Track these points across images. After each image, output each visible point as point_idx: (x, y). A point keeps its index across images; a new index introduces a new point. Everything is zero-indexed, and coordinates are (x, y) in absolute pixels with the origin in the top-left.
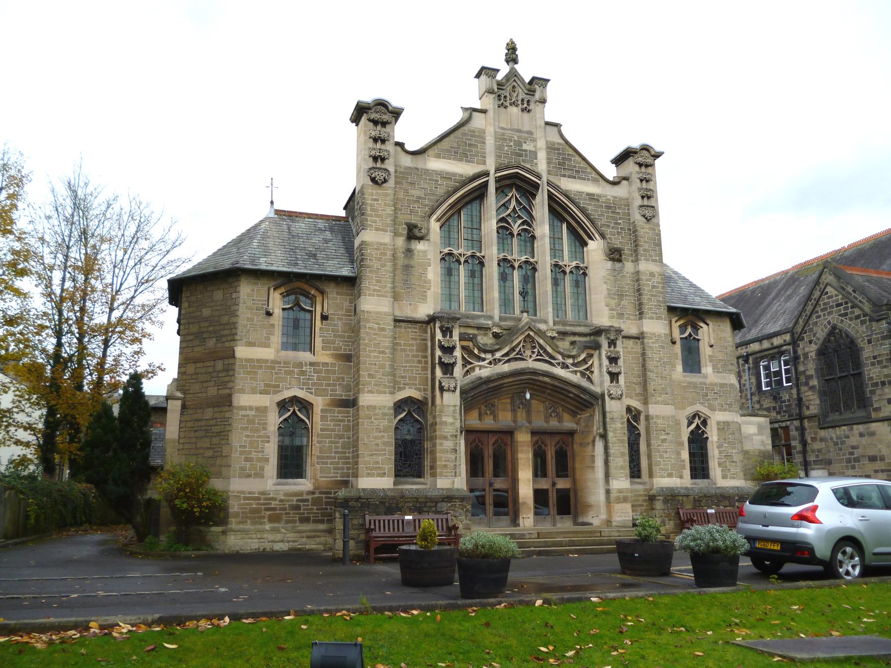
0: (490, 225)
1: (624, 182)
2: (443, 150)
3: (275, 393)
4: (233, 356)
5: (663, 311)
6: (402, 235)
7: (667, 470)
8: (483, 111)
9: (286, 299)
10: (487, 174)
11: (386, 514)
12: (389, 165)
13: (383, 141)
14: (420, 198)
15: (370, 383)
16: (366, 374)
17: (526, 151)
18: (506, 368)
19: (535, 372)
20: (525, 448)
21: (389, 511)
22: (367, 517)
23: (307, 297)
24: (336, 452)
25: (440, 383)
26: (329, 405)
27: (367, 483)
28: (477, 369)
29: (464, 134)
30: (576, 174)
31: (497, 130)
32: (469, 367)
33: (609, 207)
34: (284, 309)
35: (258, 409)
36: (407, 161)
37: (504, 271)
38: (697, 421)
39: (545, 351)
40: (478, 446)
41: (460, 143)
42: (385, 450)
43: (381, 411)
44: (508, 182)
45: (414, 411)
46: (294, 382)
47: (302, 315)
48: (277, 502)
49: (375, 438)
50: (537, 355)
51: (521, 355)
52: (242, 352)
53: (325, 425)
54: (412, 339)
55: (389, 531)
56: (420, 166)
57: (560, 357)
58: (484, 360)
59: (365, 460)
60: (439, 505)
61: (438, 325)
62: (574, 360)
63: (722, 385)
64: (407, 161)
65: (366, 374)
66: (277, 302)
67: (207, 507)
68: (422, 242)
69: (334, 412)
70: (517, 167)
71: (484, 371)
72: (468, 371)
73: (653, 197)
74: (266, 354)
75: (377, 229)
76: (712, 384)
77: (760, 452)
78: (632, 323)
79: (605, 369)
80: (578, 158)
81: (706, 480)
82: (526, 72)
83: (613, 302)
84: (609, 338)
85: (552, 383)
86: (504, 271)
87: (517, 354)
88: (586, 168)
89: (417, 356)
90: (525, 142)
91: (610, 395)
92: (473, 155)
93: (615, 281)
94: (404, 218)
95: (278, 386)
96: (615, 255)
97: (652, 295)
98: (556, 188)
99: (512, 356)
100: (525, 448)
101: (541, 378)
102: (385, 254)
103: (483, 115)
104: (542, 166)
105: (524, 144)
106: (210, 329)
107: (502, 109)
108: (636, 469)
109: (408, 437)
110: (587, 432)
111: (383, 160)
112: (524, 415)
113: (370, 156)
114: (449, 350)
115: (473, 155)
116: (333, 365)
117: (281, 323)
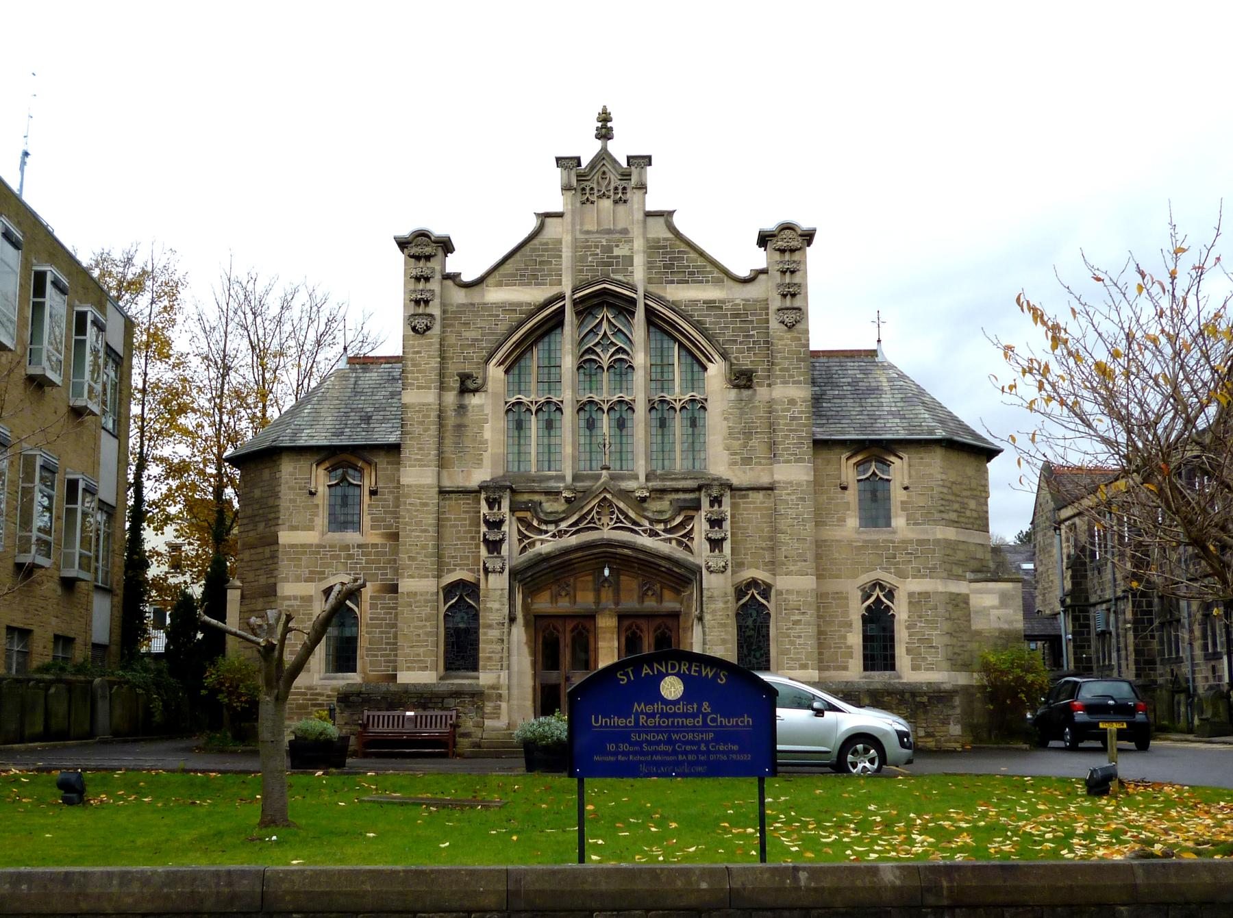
0: (568, 362)
1: (762, 277)
2: (505, 276)
3: (320, 580)
4: (275, 542)
5: (807, 448)
6: (453, 389)
7: (800, 659)
8: (559, 215)
9: (333, 474)
10: (561, 297)
11: (388, 710)
12: (435, 309)
13: (427, 279)
14: (476, 340)
15: (410, 567)
16: (406, 556)
17: (618, 257)
18: (573, 540)
19: (609, 544)
20: (608, 635)
21: (391, 707)
22: (366, 712)
23: (356, 470)
24: (387, 644)
25: (485, 564)
26: (379, 591)
27: (406, 677)
28: (538, 544)
29: (534, 250)
30: (689, 277)
31: (579, 236)
32: (526, 542)
33: (737, 316)
34: (329, 486)
35: (302, 598)
36: (459, 297)
37: (591, 416)
38: (877, 592)
39: (627, 517)
40: (636, 633)
41: (528, 263)
42: (427, 641)
43: (423, 598)
44: (595, 301)
45: (468, 595)
46: (340, 566)
47: (350, 491)
48: (324, 698)
49: (415, 627)
50: (616, 523)
51: (595, 523)
52: (286, 537)
53: (375, 613)
54: (464, 512)
55: (431, 726)
56: (476, 300)
57: (646, 523)
58: (546, 532)
59: (406, 650)
60: (446, 701)
61: (483, 496)
62: (666, 525)
63: (921, 542)
64: (459, 297)
65: (406, 556)
66: (321, 479)
67: (246, 702)
68: (477, 394)
69: (385, 600)
70: (604, 282)
71: (545, 545)
72: (525, 547)
73: (799, 293)
74: (310, 537)
75: (419, 388)
76: (903, 542)
77: (1002, 631)
78: (763, 470)
79: (703, 536)
80: (693, 255)
81: (888, 673)
82: (620, 150)
83: (736, 444)
84: (710, 496)
85: (634, 555)
86: (591, 416)
87: (589, 523)
88: (705, 267)
89: (470, 532)
90: (617, 246)
91: (708, 568)
92: (545, 275)
93: (742, 414)
94: (454, 368)
95: (323, 573)
96: (742, 380)
97: (791, 431)
98: (660, 300)
99: (581, 526)
100: (608, 635)
101: (619, 551)
102: (428, 416)
103: (559, 220)
104: (638, 275)
105: (615, 249)
106: (261, 512)
107: (588, 205)
108: (764, 659)
109: (461, 625)
110: (688, 614)
111: (427, 302)
112: (611, 595)
113: (411, 300)
114: (496, 525)
115: (545, 275)
116: (383, 546)
117: (326, 502)
